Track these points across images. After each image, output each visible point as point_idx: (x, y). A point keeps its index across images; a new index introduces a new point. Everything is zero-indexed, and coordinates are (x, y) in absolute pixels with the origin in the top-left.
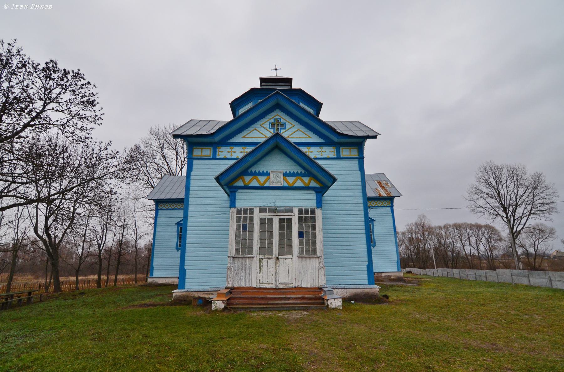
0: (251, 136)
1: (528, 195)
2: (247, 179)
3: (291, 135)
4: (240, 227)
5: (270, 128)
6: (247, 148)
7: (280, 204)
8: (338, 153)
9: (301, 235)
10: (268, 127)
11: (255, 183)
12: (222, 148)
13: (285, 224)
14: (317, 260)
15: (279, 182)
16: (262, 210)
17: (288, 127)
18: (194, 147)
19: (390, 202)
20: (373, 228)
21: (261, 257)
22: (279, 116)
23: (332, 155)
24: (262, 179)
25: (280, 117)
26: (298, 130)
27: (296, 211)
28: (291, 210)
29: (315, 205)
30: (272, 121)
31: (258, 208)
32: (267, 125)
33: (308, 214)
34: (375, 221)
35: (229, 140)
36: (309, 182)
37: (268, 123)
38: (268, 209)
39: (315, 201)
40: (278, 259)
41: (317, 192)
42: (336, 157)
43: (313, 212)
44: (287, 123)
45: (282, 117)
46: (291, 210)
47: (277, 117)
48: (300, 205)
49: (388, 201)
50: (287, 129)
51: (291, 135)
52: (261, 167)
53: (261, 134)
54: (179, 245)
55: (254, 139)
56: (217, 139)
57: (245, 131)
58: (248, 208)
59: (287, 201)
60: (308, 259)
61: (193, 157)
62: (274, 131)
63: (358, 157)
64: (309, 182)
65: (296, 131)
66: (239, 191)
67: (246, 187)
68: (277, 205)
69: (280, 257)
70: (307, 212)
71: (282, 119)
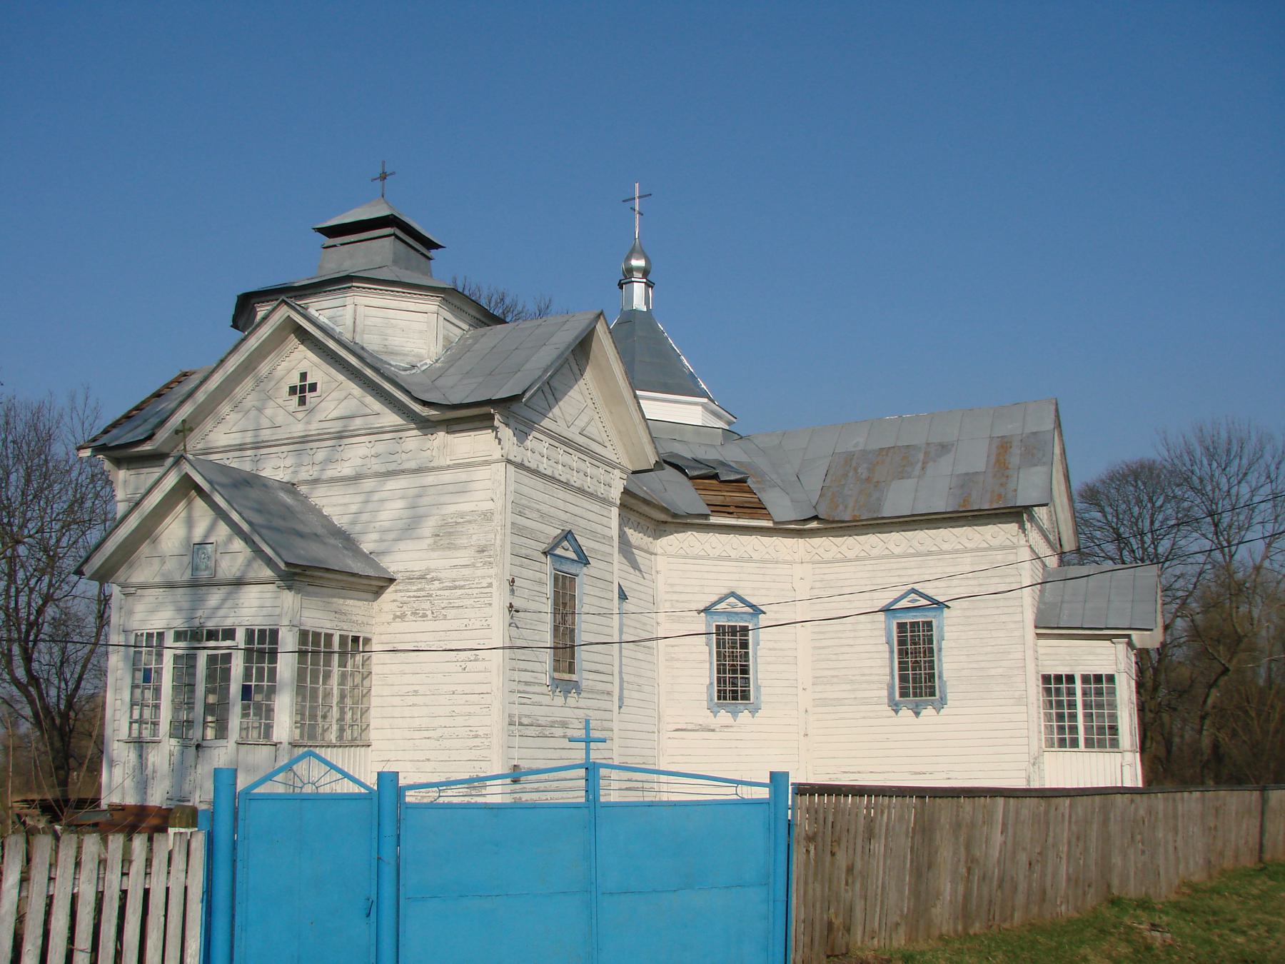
9: (246, 692)
27: (240, 635)
31: (172, 632)
33: (264, 643)
38: (189, 632)
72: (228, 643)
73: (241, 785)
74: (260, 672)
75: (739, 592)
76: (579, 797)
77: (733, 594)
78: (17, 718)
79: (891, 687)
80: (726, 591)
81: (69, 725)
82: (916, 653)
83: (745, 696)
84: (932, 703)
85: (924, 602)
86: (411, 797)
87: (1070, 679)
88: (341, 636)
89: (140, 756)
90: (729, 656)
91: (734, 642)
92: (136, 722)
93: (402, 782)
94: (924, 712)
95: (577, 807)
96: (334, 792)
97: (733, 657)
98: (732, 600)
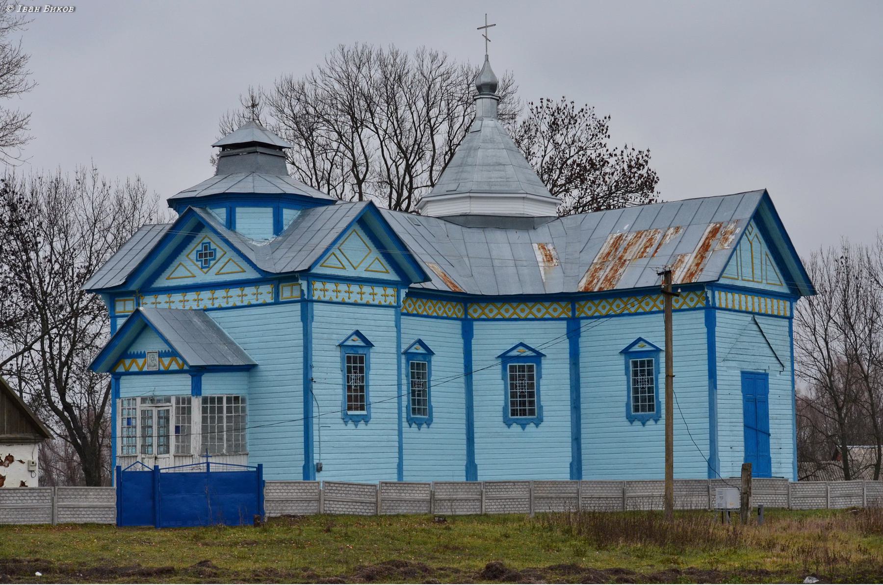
0: (177, 276)
1: (722, 301)
2: (128, 362)
3: (221, 269)
4: (414, 366)
5: (197, 260)
6: (173, 295)
7: (160, 393)
8: (277, 294)
10: (195, 259)
11: (134, 369)
12: (146, 297)
13: (165, 418)
14: (245, 456)
15: (155, 366)
16: (144, 400)
17: (218, 255)
18: (116, 299)
19: (570, 306)
20: (540, 377)
21: (143, 456)
22: (209, 238)
23: (269, 299)
24: (140, 361)
25: (210, 239)
26: (230, 260)
28: (168, 400)
29: (190, 392)
30: (199, 248)
32: (193, 256)
33: (185, 404)
34: (545, 356)
35: (153, 284)
36: (170, 364)
37: (195, 252)
39: (190, 388)
40: (156, 458)
41: (193, 376)
42: (273, 301)
43: (189, 402)
44: (218, 250)
45: (212, 239)
46: (168, 400)
47: (206, 240)
48: (177, 393)
49: (563, 304)
50: (217, 259)
51: (221, 269)
52: (136, 349)
53: (188, 270)
54: (533, 380)
55: (179, 280)
56: (134, 287)
57: (169, 268)
58: (226, 396)
59: (165, 388)
60: (184, 458)
61: (117, 314)
62: (202, 263)
63: (300, 299)
64: (170, 364)
65: (228, 262)
66: (123, 377)
67: (128, 373)
68: (157, 393)
69: (159, 456)
70: (184, 399)
71: (212, 243)
72: (168, 404)
73: (122, 469)
74: (183, 419)
75: (526, 342)
76: (205, 471)
77: (522, 344)
78: (40, 372)
79: (628, 405)
80: (517, 342)
81: (98, 442)
82: (522, 386)
83: (532, 412)
84: (532, 421)
85: (529, 353)
86: (162, 471)
87: (220, 400)
88: (227, 398)
89: (575, 407)
90: (519, 386)
91: (524, 376)
92: (162, 427)
93: (160, 468)
94: (648, 423)
95: (205, 473)
96: (629, 508)
97: (522, 386)
98: (521, 348)
